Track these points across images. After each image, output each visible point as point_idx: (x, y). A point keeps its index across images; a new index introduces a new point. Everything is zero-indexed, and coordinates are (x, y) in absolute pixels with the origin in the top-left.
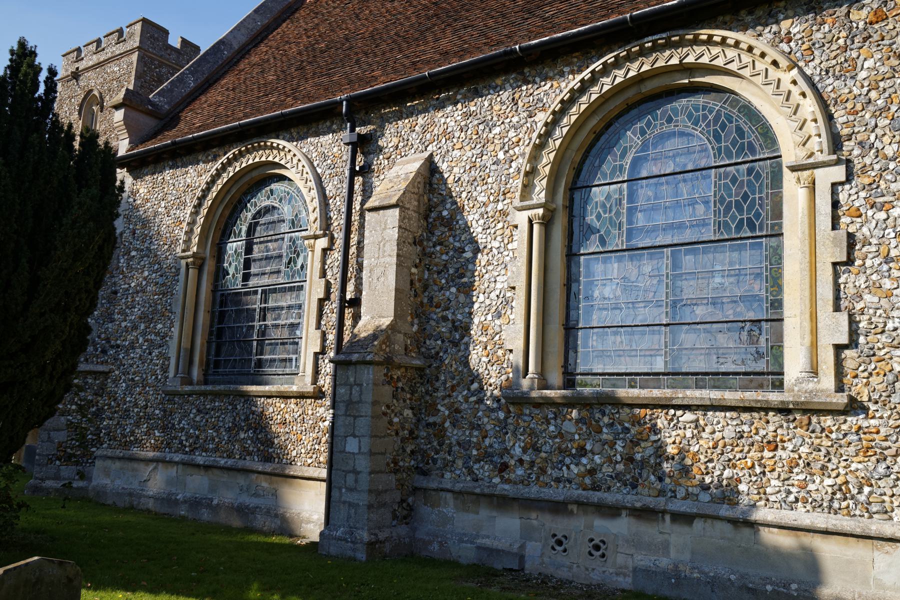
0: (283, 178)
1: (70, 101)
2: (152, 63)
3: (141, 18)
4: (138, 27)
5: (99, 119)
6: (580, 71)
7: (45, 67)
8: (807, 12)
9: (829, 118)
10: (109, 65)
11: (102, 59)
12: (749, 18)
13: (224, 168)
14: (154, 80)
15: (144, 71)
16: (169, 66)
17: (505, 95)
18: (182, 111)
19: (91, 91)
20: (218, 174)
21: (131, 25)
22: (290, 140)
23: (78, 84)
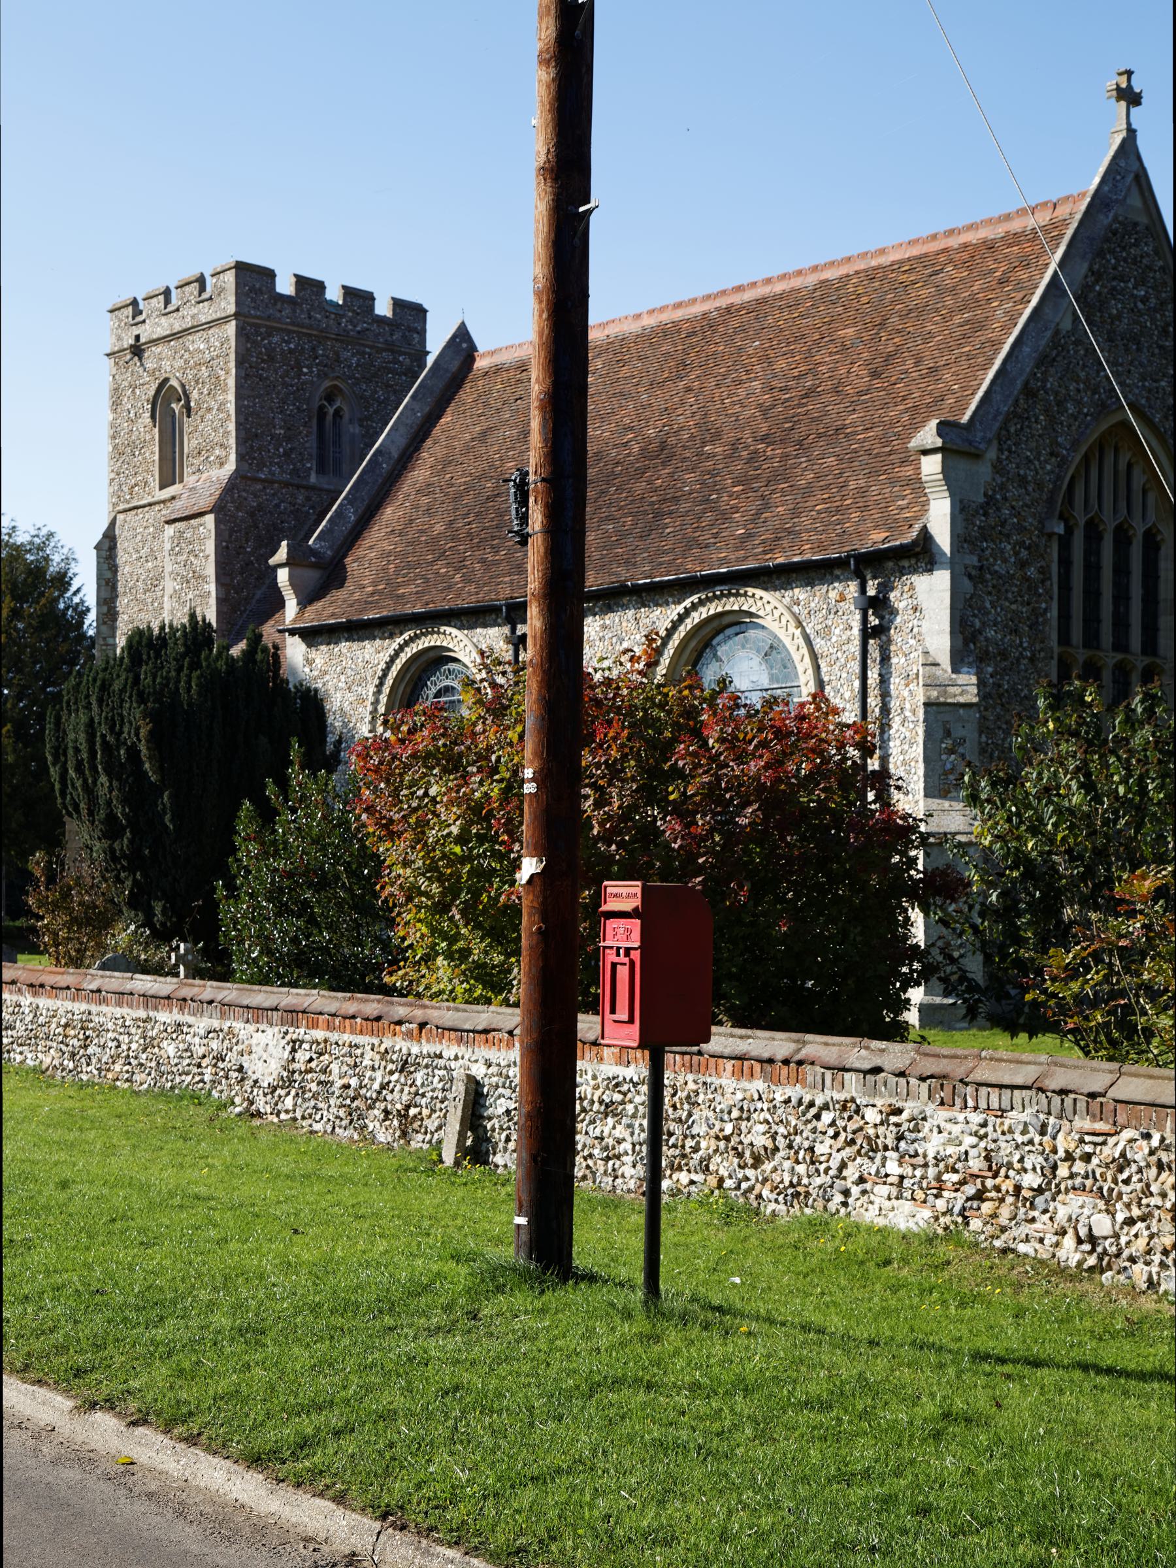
0: (456, 660)
1: (133, 392)
2: (257, 333)
3: (231, 261)
4: (230, 277)
5: (186, 429)
6: (679, 603)
7: (270, 645)
8: (807, 586)
9: (817, 668)
10: (190, 338)
11: (177, 328)
12: (777, 582)
13: (401, 648)
14: (263, 361)
15: (248, 350)
16: (282, 330)
17: (630, 613)
18: (345, 556)
19: (166, 380)
20: (397, 654)
21: (219, 273)
22: (460, 628)
23: (142, 365)
